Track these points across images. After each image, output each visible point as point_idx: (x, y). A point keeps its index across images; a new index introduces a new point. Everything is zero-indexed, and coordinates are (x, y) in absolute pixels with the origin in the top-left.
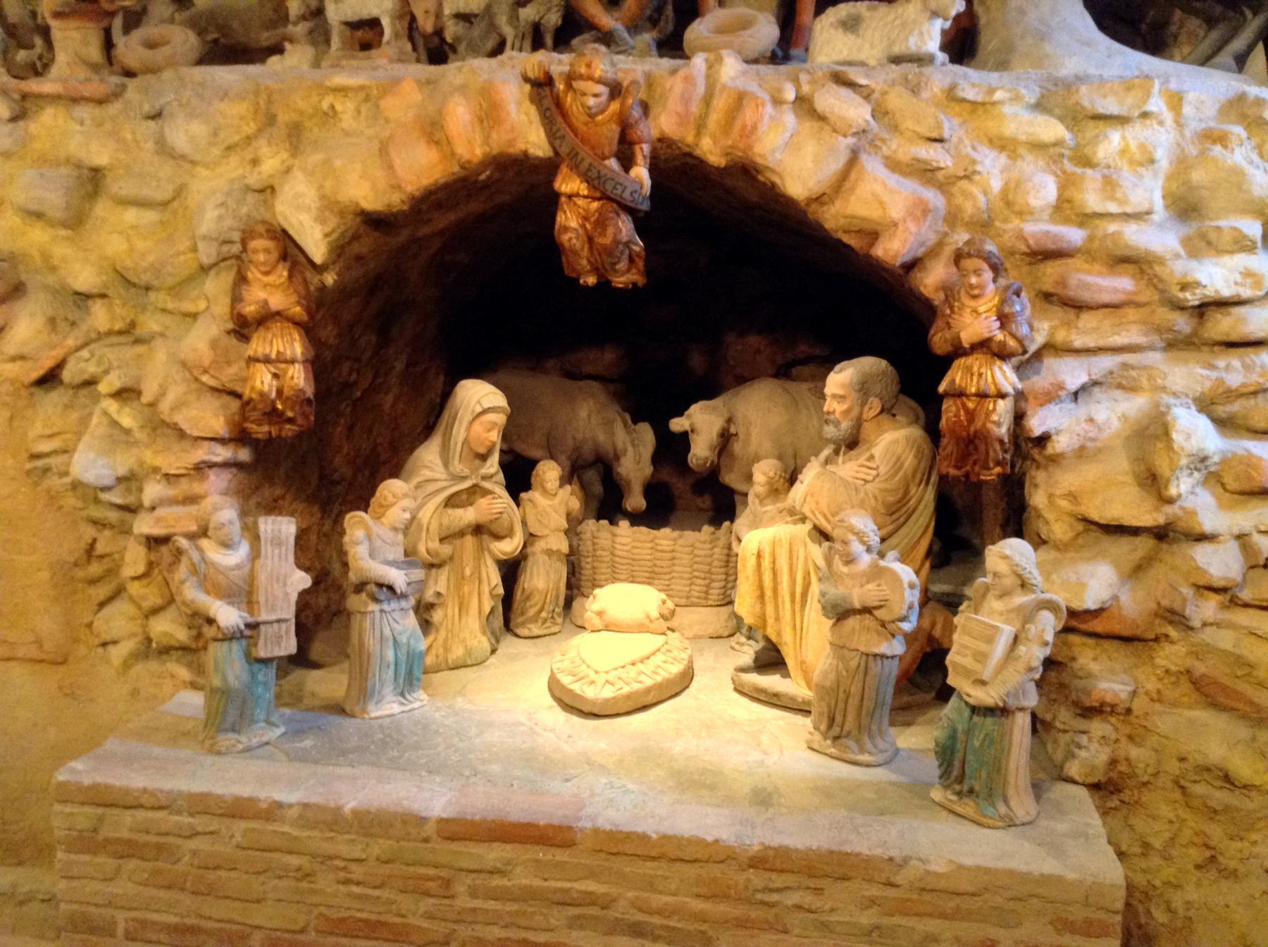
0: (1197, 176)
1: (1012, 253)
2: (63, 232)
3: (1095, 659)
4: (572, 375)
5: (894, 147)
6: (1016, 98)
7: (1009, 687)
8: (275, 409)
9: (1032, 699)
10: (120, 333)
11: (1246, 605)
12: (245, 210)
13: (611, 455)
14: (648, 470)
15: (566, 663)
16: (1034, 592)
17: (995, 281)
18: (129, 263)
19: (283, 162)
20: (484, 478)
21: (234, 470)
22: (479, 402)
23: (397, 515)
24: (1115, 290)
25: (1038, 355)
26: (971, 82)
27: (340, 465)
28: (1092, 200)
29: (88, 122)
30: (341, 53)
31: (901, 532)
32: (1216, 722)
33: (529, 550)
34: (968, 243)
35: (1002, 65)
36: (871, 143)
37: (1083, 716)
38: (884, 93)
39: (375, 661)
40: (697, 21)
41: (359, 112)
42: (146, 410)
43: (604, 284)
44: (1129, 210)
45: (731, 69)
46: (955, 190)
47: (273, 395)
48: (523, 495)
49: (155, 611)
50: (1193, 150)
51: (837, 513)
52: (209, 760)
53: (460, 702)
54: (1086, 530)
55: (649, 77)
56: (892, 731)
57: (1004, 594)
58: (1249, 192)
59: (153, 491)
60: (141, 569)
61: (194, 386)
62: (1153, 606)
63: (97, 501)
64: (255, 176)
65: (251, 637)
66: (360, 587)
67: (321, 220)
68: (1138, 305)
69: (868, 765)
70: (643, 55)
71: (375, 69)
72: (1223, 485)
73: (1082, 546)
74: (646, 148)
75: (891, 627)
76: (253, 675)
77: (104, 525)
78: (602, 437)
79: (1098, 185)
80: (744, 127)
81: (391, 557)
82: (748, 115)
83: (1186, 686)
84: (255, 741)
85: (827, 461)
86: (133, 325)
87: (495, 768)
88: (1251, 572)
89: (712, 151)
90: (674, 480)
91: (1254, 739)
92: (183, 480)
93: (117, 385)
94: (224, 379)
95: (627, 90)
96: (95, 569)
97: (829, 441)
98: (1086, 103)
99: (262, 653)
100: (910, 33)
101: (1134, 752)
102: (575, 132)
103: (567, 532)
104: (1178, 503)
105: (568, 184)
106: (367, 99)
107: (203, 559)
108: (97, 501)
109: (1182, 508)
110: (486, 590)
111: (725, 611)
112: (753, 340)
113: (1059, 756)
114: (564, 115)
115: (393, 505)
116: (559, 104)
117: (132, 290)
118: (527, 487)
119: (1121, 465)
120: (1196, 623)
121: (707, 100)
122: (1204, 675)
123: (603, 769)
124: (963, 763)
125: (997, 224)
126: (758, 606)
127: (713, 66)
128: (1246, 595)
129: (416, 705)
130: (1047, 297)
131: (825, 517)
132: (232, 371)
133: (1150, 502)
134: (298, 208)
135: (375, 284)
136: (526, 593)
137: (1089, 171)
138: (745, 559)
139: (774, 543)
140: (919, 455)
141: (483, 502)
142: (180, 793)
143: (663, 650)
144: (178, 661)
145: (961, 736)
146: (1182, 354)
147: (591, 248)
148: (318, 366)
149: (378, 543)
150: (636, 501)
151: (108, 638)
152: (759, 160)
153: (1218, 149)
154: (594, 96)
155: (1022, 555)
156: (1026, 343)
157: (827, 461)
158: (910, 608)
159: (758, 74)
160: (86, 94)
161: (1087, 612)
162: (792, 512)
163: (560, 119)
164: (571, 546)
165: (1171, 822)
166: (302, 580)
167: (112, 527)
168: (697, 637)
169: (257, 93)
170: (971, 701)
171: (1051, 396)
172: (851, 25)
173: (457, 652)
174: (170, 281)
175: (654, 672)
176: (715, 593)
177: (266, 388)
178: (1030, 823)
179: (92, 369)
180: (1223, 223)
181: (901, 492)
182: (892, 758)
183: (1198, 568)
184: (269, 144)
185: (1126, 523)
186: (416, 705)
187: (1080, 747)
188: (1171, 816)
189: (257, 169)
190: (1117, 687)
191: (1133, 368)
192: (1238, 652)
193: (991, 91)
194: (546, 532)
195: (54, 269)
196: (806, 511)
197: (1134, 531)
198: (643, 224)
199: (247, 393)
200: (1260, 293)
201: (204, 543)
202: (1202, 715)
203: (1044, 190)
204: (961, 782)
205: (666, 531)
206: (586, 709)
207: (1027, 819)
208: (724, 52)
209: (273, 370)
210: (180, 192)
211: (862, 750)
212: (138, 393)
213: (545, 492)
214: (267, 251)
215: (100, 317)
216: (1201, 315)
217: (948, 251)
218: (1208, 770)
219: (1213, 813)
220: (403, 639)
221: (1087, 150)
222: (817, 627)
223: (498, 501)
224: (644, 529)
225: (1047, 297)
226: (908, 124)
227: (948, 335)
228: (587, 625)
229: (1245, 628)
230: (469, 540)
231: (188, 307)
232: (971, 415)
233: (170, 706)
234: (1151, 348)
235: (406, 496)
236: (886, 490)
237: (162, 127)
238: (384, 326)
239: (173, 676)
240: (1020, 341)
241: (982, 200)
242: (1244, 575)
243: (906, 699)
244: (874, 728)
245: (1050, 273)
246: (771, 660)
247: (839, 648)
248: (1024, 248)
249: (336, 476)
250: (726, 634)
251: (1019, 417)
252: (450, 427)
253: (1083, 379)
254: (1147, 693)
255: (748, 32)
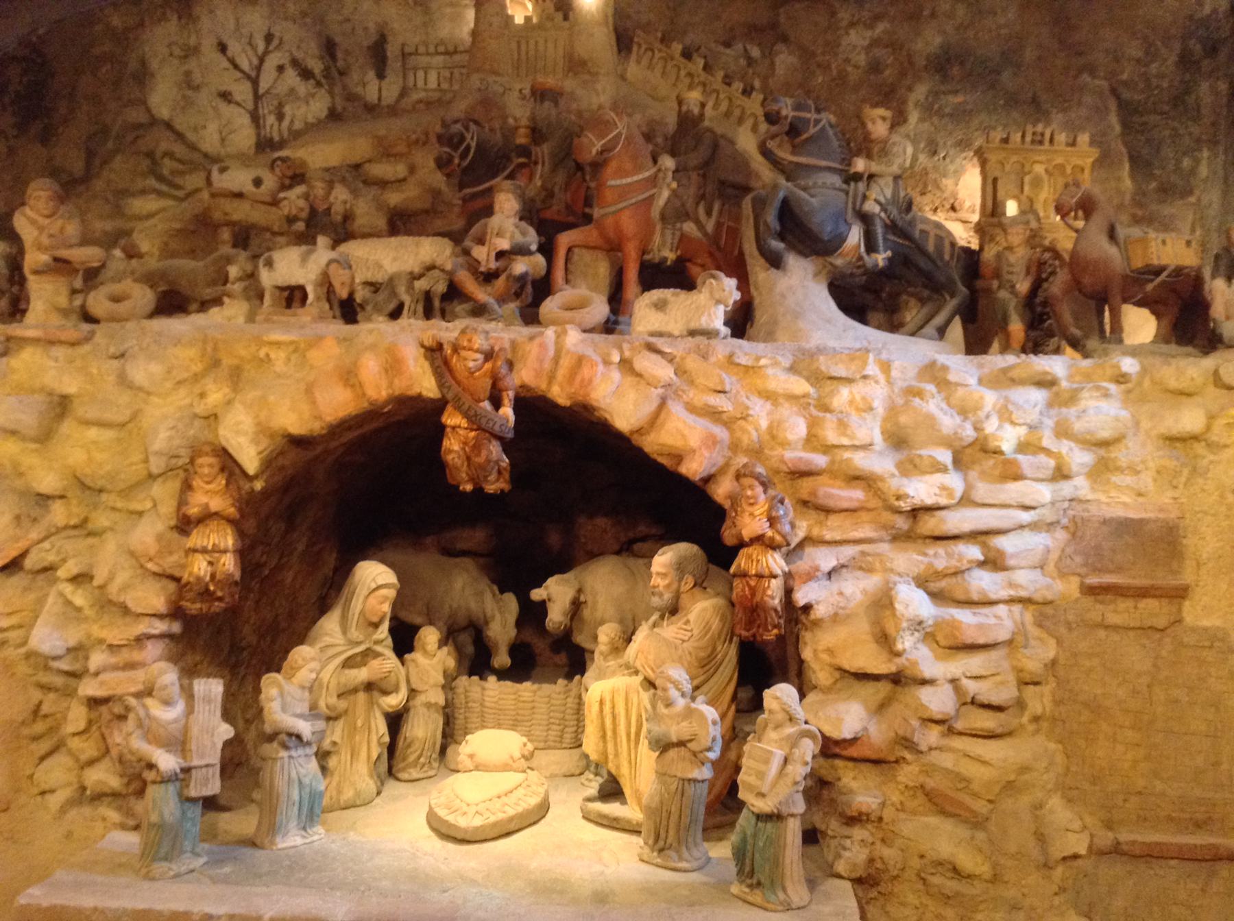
0: (903, 419)
1: (777, 472)
2: (34, 446)
3: (854, 778)
4: (450, 552)
5: (691, 395)
6: (776, 364)
7: (781, 798)
8: (207, 590)
9: (800, 806)
10: (75, 527)
11: (961, 734)
12: (192, 432)
13: (482, 621)
14: (513, 632)
15: (443, 799)
16: (797, 723)
17: (765, 492)
18: (88, 471)
19: (225, 395)
20: (377, 642)
21: (167, 641)
22: (374, 580)
23: (305, 675)
24: (851, 499)
25: (801, 545)
26: (745, 350)
27: (248, 634)
28: (831, 435)
29: (61, 359)
30: (271, 309)
31: (712, 681)
32: (946, 826)
33: (411, 703)
34: (745, 466)
35: (769, 337)
36: (675, 392)
37: (847, 824)
38: (683, 359)
39: (283, 799)
40: (549, 298)
41: (289, 360)
42: (97, 591)
43: (479, 490)
44: (857, 443)
45: (573, 337)
46: (735, 427)
47: (208, 578)
48: (407, 656)
49: (91, 763)
50: (900, 401)
51: (659, 667)
52: (146, 885)
53: (352, 836)
54: (842, 678)
55: (514, 344)
56: (706, 845)
57: (778, 727)
58: (939, 431)
59: (97, 659)
60: (82, 725)
61: (139, 571)
62: (892, 734)
63: (47, 668)
64: (202, 406)
65: (183, 780)
66: (272, 738)
67: (255, 441)
68: (869, 510)
69: (685, 871)
70: (509, 324)
71: (302, 327)
72: (937, 643)
73: (840, 690)
74: (511, 394)
75: (699, 756)
76: (184, 813)
77: (50, 689)
78: (473, 605)
79: (834, 425)
80: (583, 380)
81: (299, 711)
82: (586, 372)
83: (921, 798)
84: (183, 869)
85: (654, 625)
86: (86, 520)
87: (385, 884)
88: (964, 708)
89: (560, 395)
90: (535, 641)
91: (972, 838)
92: (124, 650)
93: (75, 571)
94: (166, 566)
95: (497, 355)
96: (39, 727)
97: (656, 609)
98: (823, 368)
99: (193, 793)
100: (703, 314)
101: (887, 852)
102: (459, 383)
103: (443, 687)
104: (905, 656)
105: (451, 419)
106: (295, 351)
107: (148, 715)
108: (47, 668)
109: (907, 660)
110: (374, 739)
111: (576, 752)
112: (601, 522)
113: (830, 858)
114: (451, 371)
115: (300, 668)
116: (446, 363)
117: (88, 492)
118: (410, 648)
119: (863, 627)
120: (923, 748)
121: (556, 360)
122: (932, 789)
123: (473, 882)
124: (753, 861)
125: (766, 451)
126: (601, 744)
127: (560, 336)
128: (959, 725)
129: (316, 838)
130: (805, 503)
131: (652, 669)
132: (174, 558)
133: (885, 655)
134: (238, 432)
135: (287, 486)
136: (408, 740)
137: (828, 415)
138: (590, 706)
139: (613, 693)
140: (723, 619)
141: (375, 663)
142: (125, 910)
143: (524, 785)
144: (109, 805)
145: (750, 840)
146: (902, 545)
147: (469, 465)
148: (243, 554)
149: (289, 699)
150: (502, 659)
151: (47, 787)
152: (595, 404)
153: (917, 401)
154: (473, 360)
155: (788, 696)
156: (789, 538)
157: (654, 625)
158: (714, 740)
159: (593, 342)
160: (63, 338)
161: (845, 741)
162: (627, 666)
163: (447, 374)
164: (446, 700)
165: (917, 908)
166: (226, 731)
167: (56, 690)
168: (552, 776)
169: (205, 342)
170: (755, 810)
171: (810, 576)
172: (660, 306)
173: (348, 794)
174: (122, 486)
175: (517, 804)
176: (568, 737)
177: (202, 573)
178: (803, 907)
179: (51, 558)
180: (924, 452)
181: (710, 649)
182: (705, 864)
183: (922, 705)
184: (215, 381)
185: (869, 671)
186: (316, 838)
187: (845, 849)
188: (917, 902)
189: (204, 401)
190: (869, 800)
191: (869, 555)
192: (956, 769)
193: (758, 359)
194: (426, 688)
195: (21, 475)
196: (638, 665)
197: (876, 678)
198: (507, 447)
199: (185, 578)
200: (953, 502)
201: (149, 701)
202: (934, 820)
203: (797, 428)
204: (752, 877)
205: (527, 684)
206: (459, 836)
207: (802, 904)
208: (568, 326)
209: (208, 558)
210: (135, 416)
211: (681, 859)
212: (92, 578)
213: (425, 652)
214: (210, 466)
215: (59, 514)
216: (915, 517)
217: (732, 470)
218: (941, 864)
219: (947, 899)
220: (306, 781)
221: (827, 400)
222: (647, 757)
223: (389, 661)
224: (509, 683)
225: (805, 503)
226: (700, 380)
227: (734, 531)
228: (460, 767)
229: (959, 751)
230: (362, 696)
231: (139, 507)
232: (753, 591)
233: (103, 844)
234: (881, 540)
235: (313, 659)
236: (701, 648)
237: (123, 365)
238: (290, 517)
239: (104, 819)
240: (784, 537)
241: (754, 435)
242: (958, 711)
243: (719, 819)
244: (690, 840)
245: (806, 485)
246: (612, 791)
247: (661, 775)
248: (785, 469)
249: (244, 644)
250: (578, 772)
251: (788, 592)
252: (348, 601)
253: (833, 563)
254: (893, 805)
255: (586, 310)
